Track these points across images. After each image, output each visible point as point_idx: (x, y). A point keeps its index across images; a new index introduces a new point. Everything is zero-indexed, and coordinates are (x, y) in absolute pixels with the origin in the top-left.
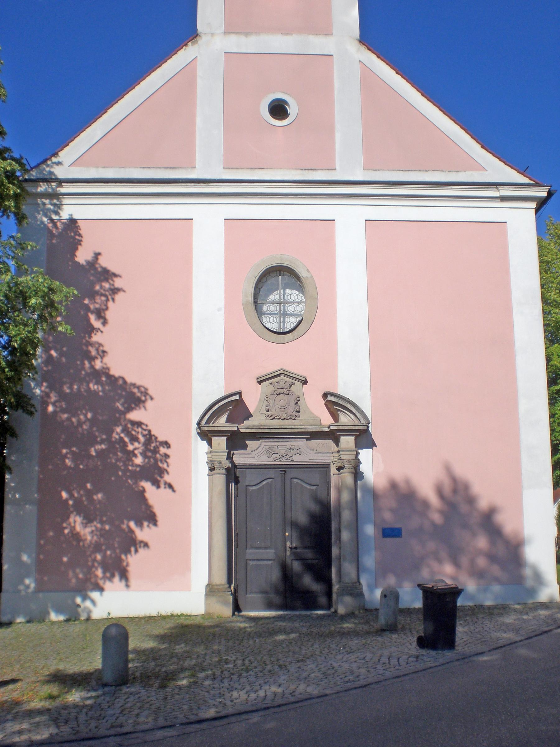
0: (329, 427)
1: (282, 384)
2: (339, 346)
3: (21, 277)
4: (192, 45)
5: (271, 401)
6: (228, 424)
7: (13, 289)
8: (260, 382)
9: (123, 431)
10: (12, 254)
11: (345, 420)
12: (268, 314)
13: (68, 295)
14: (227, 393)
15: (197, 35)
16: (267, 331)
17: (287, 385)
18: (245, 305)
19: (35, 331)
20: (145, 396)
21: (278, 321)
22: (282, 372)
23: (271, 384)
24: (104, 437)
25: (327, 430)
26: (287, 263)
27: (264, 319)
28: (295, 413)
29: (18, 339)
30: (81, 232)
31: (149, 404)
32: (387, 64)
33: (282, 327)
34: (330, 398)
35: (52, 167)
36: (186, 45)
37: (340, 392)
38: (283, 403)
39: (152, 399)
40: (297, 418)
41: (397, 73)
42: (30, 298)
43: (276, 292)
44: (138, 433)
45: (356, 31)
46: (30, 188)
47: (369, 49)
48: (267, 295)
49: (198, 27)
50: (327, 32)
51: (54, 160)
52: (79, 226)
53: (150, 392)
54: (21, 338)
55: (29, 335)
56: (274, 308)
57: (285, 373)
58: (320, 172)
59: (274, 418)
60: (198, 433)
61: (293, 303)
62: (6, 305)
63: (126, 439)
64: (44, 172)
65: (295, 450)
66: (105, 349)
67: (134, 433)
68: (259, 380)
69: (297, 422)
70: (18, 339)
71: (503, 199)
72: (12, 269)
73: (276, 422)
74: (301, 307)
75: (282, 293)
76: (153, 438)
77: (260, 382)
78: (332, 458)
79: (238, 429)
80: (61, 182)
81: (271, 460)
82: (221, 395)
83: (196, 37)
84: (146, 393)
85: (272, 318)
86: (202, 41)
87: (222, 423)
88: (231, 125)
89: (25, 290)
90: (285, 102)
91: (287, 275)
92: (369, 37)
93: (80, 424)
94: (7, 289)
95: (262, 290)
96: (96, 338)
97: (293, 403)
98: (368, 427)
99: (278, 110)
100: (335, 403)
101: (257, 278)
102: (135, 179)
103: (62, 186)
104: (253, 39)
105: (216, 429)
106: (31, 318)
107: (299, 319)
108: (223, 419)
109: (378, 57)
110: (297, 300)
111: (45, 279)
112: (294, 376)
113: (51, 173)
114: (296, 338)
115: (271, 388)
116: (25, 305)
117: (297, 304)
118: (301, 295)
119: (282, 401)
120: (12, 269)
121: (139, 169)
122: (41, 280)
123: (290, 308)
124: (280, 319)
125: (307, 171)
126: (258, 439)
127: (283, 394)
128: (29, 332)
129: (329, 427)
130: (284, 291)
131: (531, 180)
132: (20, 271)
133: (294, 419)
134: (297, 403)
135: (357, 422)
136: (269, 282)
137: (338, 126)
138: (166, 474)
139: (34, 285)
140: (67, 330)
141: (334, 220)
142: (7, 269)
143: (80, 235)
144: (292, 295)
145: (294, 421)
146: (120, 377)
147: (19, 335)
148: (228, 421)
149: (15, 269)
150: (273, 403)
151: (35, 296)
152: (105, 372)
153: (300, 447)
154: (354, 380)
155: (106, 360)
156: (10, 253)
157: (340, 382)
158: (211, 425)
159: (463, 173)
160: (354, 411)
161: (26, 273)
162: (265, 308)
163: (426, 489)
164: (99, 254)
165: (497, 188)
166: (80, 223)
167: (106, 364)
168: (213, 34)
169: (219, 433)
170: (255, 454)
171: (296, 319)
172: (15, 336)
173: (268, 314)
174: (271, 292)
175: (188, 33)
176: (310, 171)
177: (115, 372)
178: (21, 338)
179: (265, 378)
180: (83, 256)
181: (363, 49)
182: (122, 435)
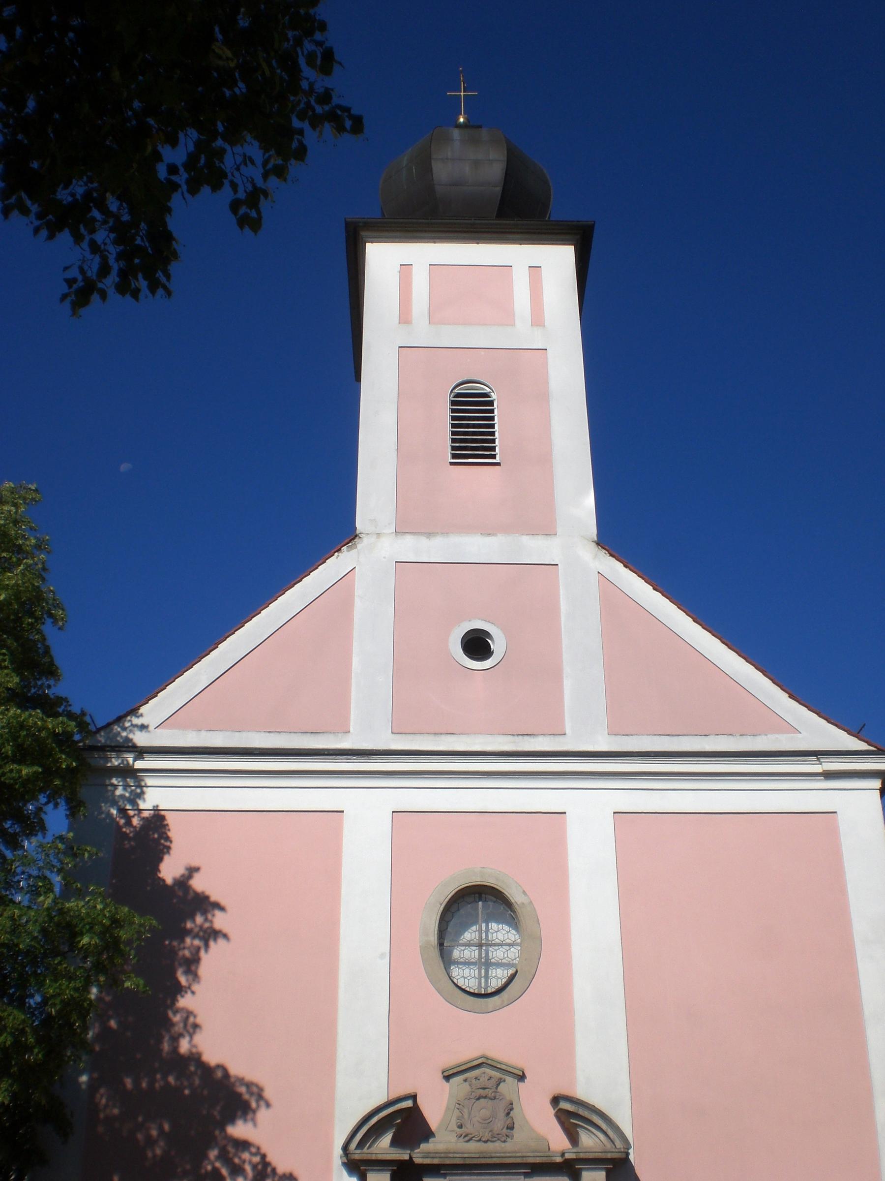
0: (563, 1154)
1: (484, 1080)
2: (577, 1017)
3: (69, 901)
4: (348, 551)
5: (466, 1111)
6: (393, 1150)
7: (56, 919)
8: (447, 1078)
9: (218, 1157)
10: (58, 865)
11: (590, 1141)
12: (462, 963)
13: (143, 930)
14: (394, 1095)
15: (356, 536)
16: (460, 992)
17: (493, 1081)
18: (424, 949)
19: (86, 989)
20: (257, 1101)
23: (465, 1080)
24: (188, 1167)
25: (559, 1159)
26: (491, 882)
27: (455, 971)
28: (505, 1130)
29: (58, 1001)
30: (170, 834)
31: (263, 1114)
32: (639, 576)
33: (483, 985)
34: (565, 1105)
35: (131, 731)
36: (339, 550)
38: (484, 1113)
39: (268, 1105)
40: (509, 1140)
41: (654, 589)
42: (82, 934)
43: (474, 928)
44: (244, 1161)
45: (592, 529)
46: (95, 759)
47: (611, 555)
48: (460, 933)
49: (358, 525)
50: (549, 531)
51: (136, 721)
52: (167, 825)
53: (268, 1094)
54: (62, 1001)
55: (76, 995)
56: (471, 954)
57: (489, 1062)
58: (540, 738)
59: (471, 1139)
60: (344, 1164)
61: (501, 945)
62: (42, 946)
63: (224, 1172)
64: (118, 739)
66: (199, 1020)
67: (236, 1160)
68: (446, 1074)
70: (58, 1001)
71: (829, 775)
72: (57, 889)
74: (514, 952)
75: (484, 929)
76: (269, 1169)
77: (447, 1078)
79: (411, 1158)
80: (141, 752)
82: (380, 1098)
83: (354, 539)
84: (260, 1097)
85: (467, 970)
86: (362, 544)
87: (383, 1146)
88: (405, 668)
89: (74, 922)
90: (487, 634)
91: (491, 901)
92: (613, 536)
93: (151, 1142)
94: (46, 919)
95: (451, 924)
96: (184, 1002)
97: (501, 1114)
98: (628, 1154)
99: (477, 645)
100: (572, 1114)
102: (256, 749)
103: (142, 758)
104: (438, 542)
105: (374, 1157)
106: (81, 967)
107: (511, 971)
108: (386, 1140)
109: (626, 566)
110: (508, 941)
111: (106, 906)
112: (504, 1067)
113: (128, 740)
114: (506, 1003)
116: (73, 946)
117: (508, 948)
118: (514, 932)
119: (483, 1109)
120: (57, 889)
121: (263, 734)
122: (99, 907)
123: (497, 954)
124: (480, 973)
125: (520, 737)
126: (444, 1176)
127: (485, 1097)
128: (76, 989)
129: (563, 1154)
130: (487, 926)
131: (869, 745)
132: (68, 892)
133: (505, 1141)
134: (508, 1114)
135: (609, 1145)
136: (462, 912)
137: (567, 670)
139: (88, 914)
140: (138, 986)
141: (565, 813)
142: (49, 889)
143: (168, 839)
144: (500, 932)
145: (503, 1145)
146: (219, 1066)
147: (59, 994)
148: (394, 1143)
149: (61, 890)
150: (470, 1114)
151: (88, 931)
152: (195, 1058)
154: (603, 1075)
155: (198, 1038)
156: (55, 862)
157: (581, 1077)
158: (365, 1150)
159: (764, 737)
160: (604, 1126)
161: (80, 894)
162: (456, 954)
164: (197, 869)
165: (818, 759)
166: (170, 819)
167: (195, 1046)
168: (378, 535)
169: (380, 1164)
171: (505, 972)
172: (53, 996)
173: (462, 963)
174: (465, 927)
175: (340, 531)
176: (526, 738)
177: (211, 1057)
178: (62, 1001)
179: (455, 1071)
180: (170, 870)
181: (603, 555)
182: (218, 1164)
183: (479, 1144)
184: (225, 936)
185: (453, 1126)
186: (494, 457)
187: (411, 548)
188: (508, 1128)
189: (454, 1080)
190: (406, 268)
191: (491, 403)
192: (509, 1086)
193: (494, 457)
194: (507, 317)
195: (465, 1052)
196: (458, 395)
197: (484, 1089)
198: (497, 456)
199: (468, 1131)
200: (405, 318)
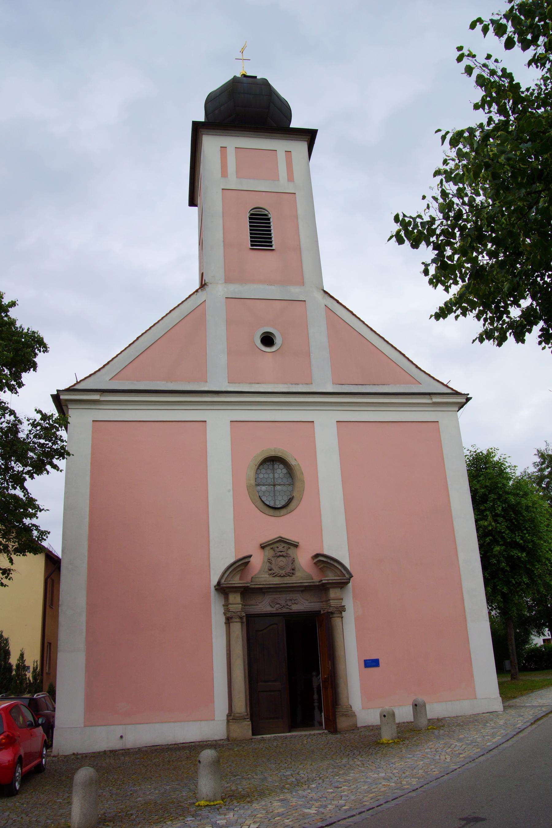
18: (249, 487)
26: (279, 454)
58: (300, 385)
65: (293, 601)
81: (274, 609)
82: (232, 560)
87: (236, 581)
97: (290, 563)
99: (268, 340)
100: (323, 562)
115: (272, 552)
119: (282, 561)
134: (292, 563)
138: (45, 472)
154: (337, 547)
160: (340, 567)
163: (438, 311)
170: (264, 606)
185: (266, 570)
186: (271, 246)
187: (236, 289)
189: (268, 549)
191: (269, 219)
193: (271, 246)
194: (276, 178)
195: (271, 535)
196: (252, 215)
198: (274, 246)
199: (274, 572)
200: (224, 173)
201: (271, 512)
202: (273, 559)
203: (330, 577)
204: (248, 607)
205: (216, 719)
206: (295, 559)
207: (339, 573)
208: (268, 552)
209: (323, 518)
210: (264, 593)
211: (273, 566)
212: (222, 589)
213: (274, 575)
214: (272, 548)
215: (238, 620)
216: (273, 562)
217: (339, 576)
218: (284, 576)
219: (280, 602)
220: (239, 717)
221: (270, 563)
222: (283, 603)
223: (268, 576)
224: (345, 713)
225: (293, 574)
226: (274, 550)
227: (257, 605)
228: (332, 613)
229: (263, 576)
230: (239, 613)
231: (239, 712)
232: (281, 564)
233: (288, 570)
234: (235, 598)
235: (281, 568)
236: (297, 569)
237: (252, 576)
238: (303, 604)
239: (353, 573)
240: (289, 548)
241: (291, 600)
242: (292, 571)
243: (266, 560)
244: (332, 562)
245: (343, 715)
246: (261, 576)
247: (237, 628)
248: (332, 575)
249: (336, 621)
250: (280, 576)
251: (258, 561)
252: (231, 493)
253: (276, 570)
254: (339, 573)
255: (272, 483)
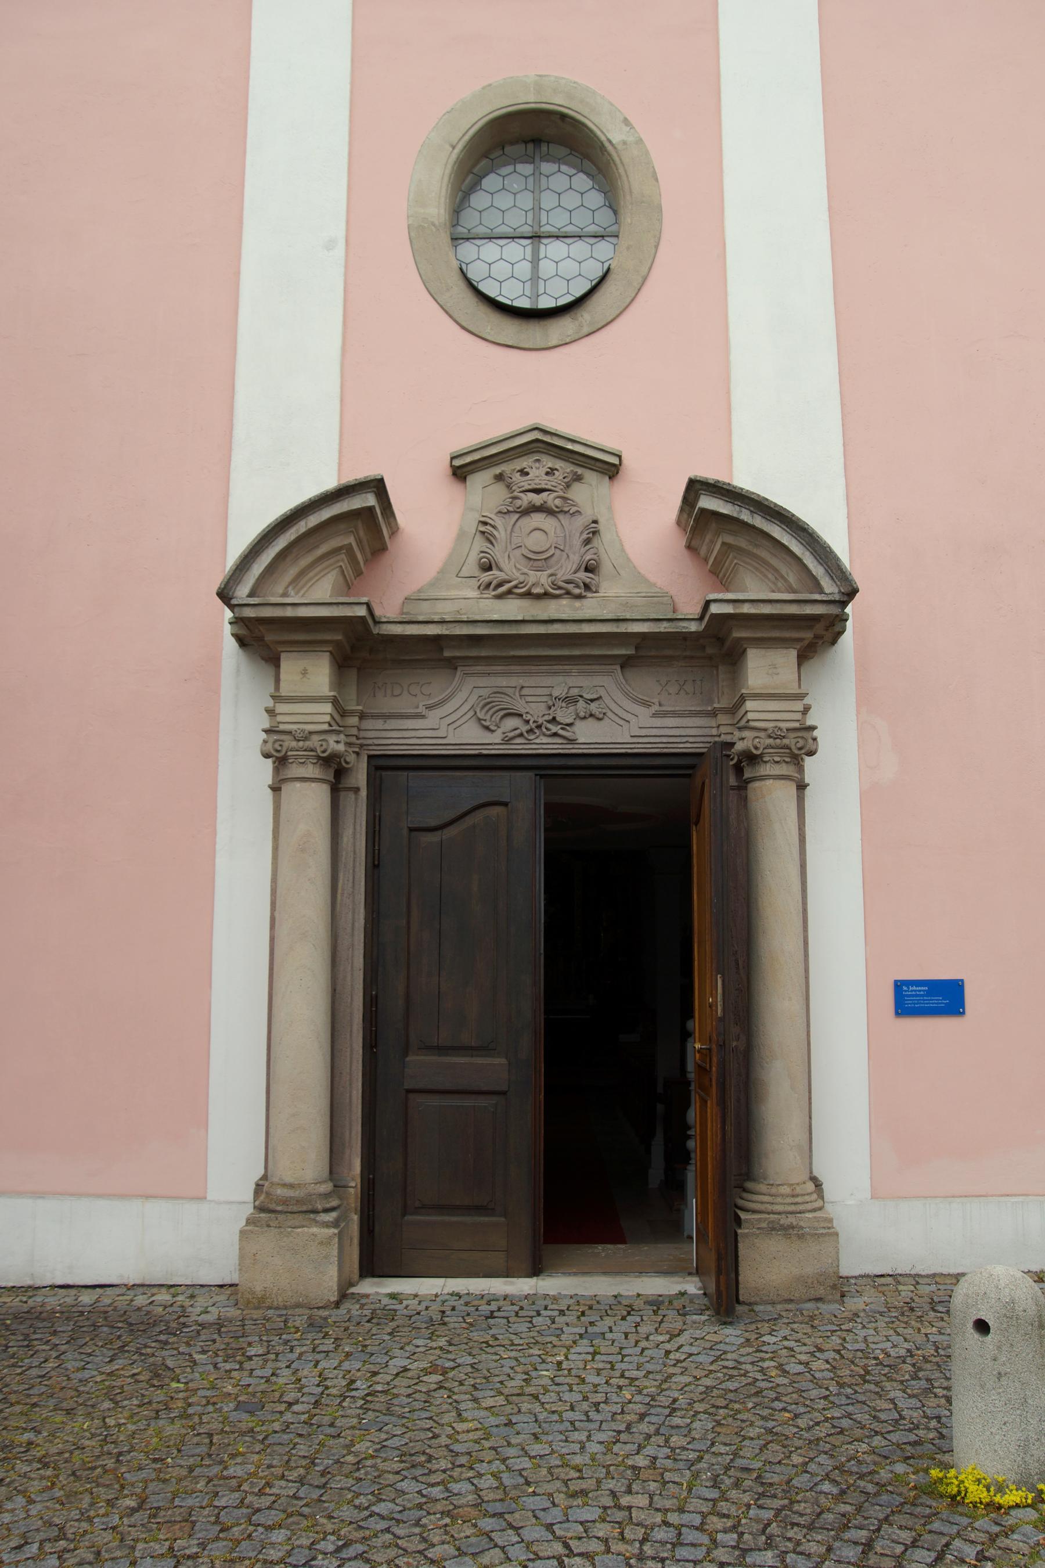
18: (417, 232)
21: (529, 257)
22: (536, 435)
34: (707, 502)
37: (743, 481)
59: (509, 592)
65: (581, 704)
68: (457, 463)
69: (588, 608)
73: (513, 609)
77: (461, 472)
78: (714, 732)
81: (496, 738)
87: (319, 594)
97: (577, 541)
100: (722, 520)
101: (460, 146)
114: (586, 330)
115: (498, 495)
133: (579, 597)
134: (587, 541)
145: (577, 603)
153: (602, 692)
154: (790, 457)
160: (796, 547)
170: (448, 719)
183: (525, 603)
184: (963, 1275)
185: (471, 567)
188: (587, 570)
189: (481, 479)
190: (800, 687)
192: (590, 494)
197: (538, 491)
199: (502, 576)
201: (509, 329)
202: (498, 522)
203: (755, 591)
204: (379, 724)
205: (209, 1198)
206: (602, 527)
207: (792, 579)
208: (484, 493)
209: (735, 356)
210: (452, 665)
211: (498, 553)
212: (263, 638)
213: (505, 591)
214: (499, 478)
215: (311, 770)
216: (501, 534)
217: (794, 592)
218: (546, 595)
219: (520, 706)
220: (285, 1201)
221: (489, 538)
222: (537, 711)
223: (475, 594)
224: (785, 1221)
225: (587, 587)
226: (509, 486)
227: (423, 717)
228: (752, 758)
229: (453, 593)
230: (315, 741)
231: (289, 1179)
232: (536, 542)
233: (566, 569)
234: (305, 672)
235: (537, 560)
236: (606, 567)
237: (406, 594)
238: (626, 720)
239: (859, 578)
240: (578, 478)
241: (570, 700)
242: (582, 575)
243: (472, 527)
244: (758, 522)
245: (774, 1228)
246: (444, 594)
247: (310, 800)
248: (765, 590)
249: (773, 797)
250: (528, 595)
251: (433, 531)
252: (340, 251)
253: (511, 568)
254: (792, 579)
255: (527, 230)
